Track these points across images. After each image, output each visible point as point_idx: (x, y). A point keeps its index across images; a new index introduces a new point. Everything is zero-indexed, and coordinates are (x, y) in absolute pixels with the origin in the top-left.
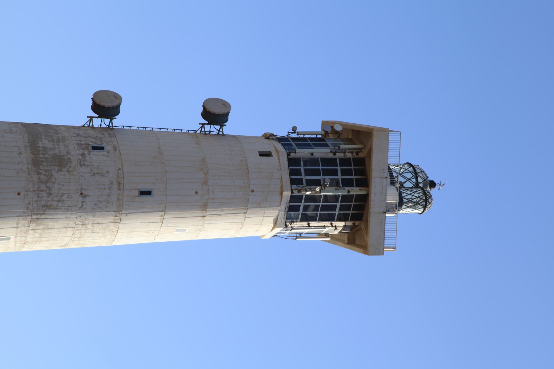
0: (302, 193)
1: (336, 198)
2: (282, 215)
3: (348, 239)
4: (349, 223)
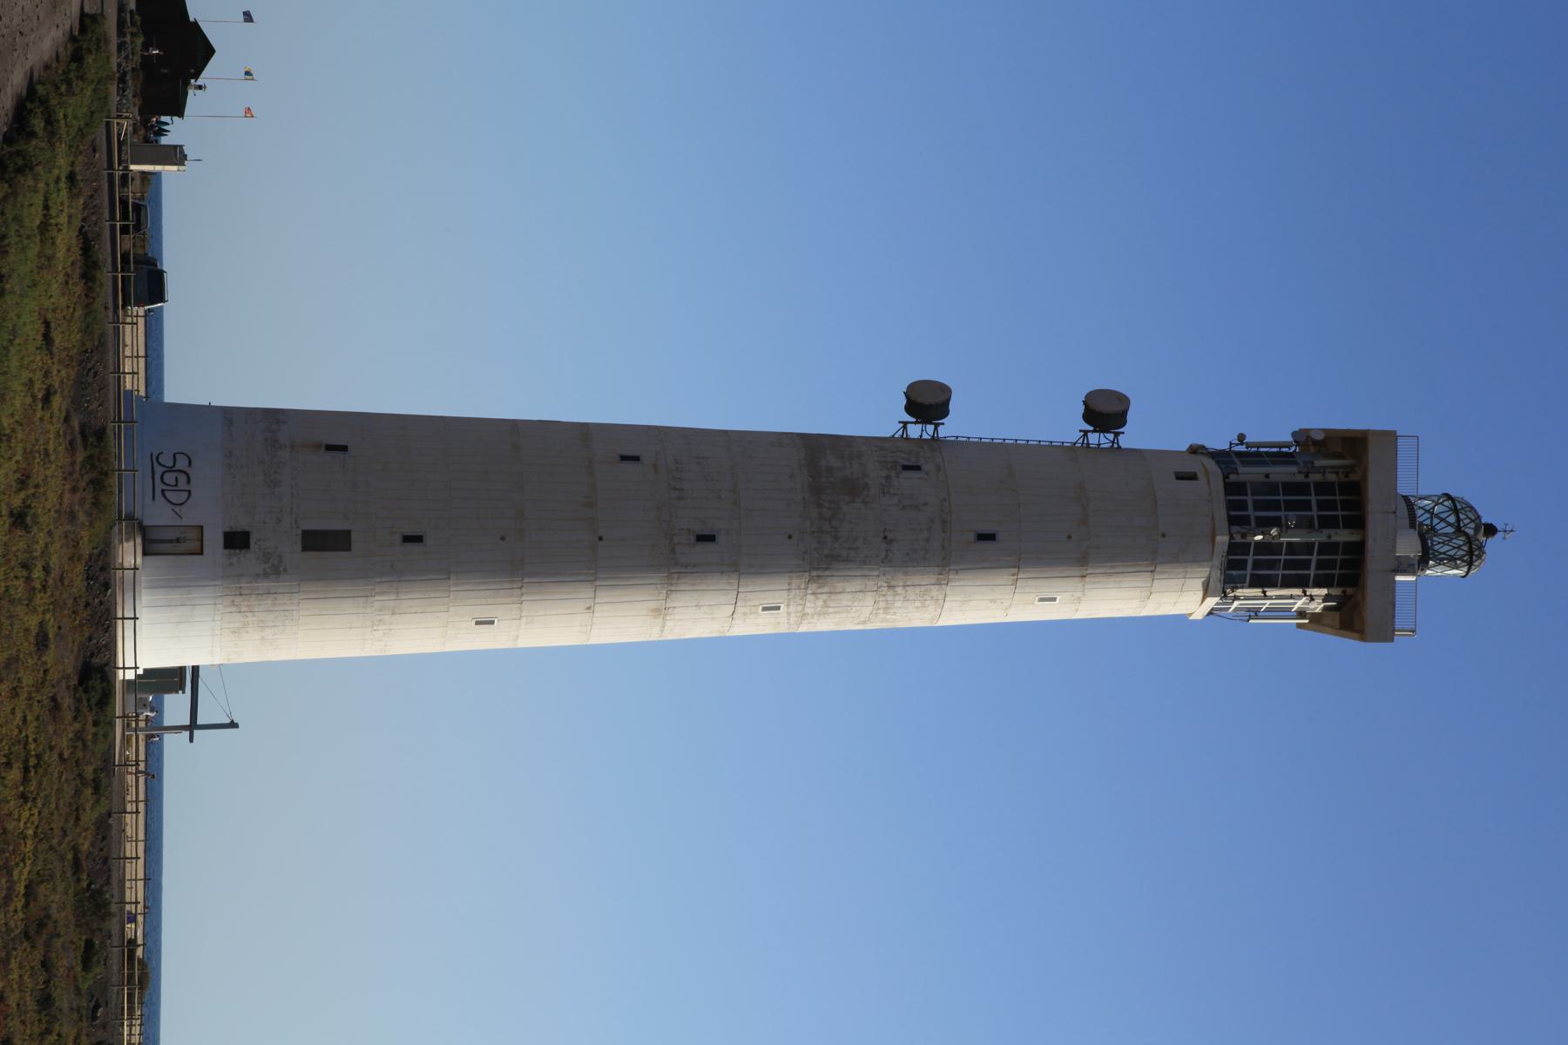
0: (1248, 539)
1: (1308, 548)
2: (1217, 574)
3: (1341, 621)
4: (1336, 591)
